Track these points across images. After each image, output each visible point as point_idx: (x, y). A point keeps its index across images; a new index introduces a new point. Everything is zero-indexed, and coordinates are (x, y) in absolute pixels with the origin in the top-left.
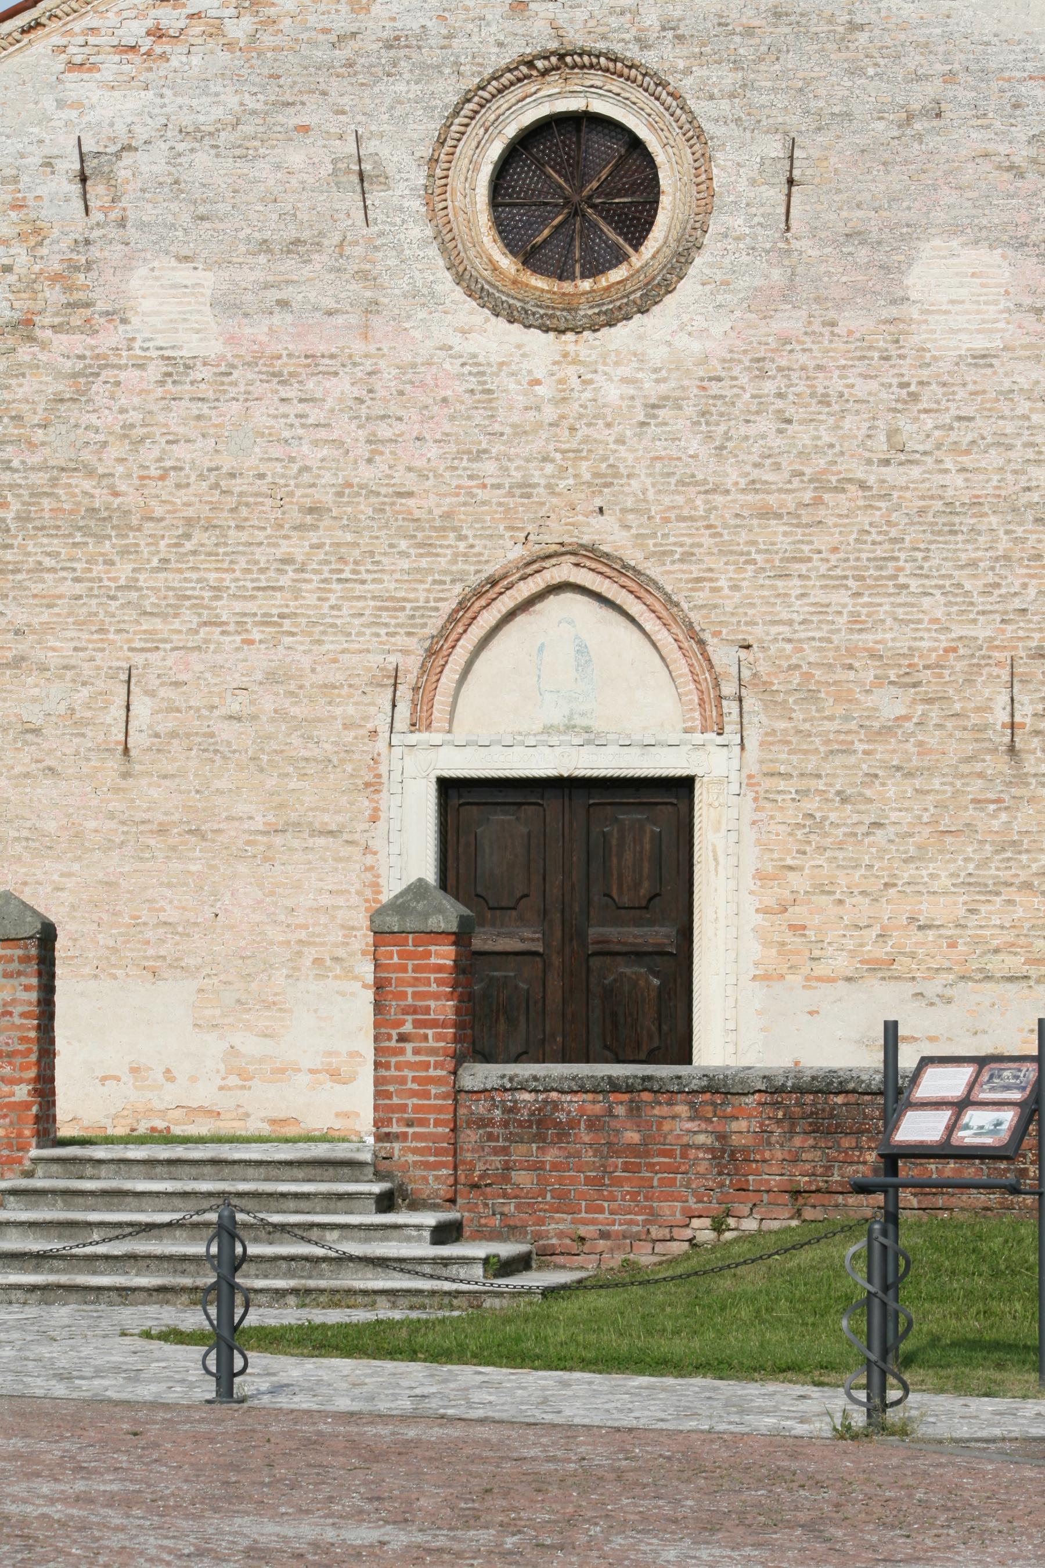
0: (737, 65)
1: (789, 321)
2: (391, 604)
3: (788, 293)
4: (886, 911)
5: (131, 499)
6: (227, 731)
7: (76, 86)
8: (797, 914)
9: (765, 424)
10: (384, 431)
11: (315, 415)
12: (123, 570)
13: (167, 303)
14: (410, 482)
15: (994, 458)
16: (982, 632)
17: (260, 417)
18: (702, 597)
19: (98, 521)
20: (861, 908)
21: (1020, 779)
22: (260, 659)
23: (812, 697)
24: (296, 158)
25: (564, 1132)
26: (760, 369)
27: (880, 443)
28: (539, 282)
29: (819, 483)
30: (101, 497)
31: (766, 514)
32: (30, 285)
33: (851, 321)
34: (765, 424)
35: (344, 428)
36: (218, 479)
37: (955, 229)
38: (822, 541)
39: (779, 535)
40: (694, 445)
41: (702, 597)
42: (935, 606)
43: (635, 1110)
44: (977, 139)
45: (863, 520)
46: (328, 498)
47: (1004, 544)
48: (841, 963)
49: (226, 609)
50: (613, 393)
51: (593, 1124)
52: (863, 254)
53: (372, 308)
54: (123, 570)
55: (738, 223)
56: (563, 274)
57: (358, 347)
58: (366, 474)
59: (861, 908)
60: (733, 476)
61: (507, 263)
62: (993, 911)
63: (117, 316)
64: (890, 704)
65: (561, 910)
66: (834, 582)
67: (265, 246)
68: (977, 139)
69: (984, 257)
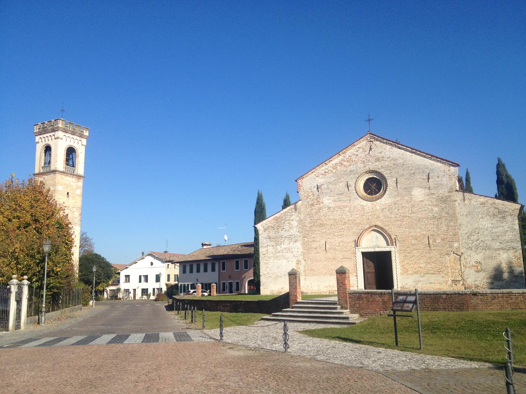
0: (390, 170)
1: (398, 198)
2: (354, 232)
3: (398, 195)
4: (415, 266)
5: (325, 222)
6: (337, 247)
7: (317, 179)
8: (405, 266)
9: (396, 210)
10: (352, 213)
11: (344, 212)
12: (325, 230)
13: (327, 201)
14: (356, 219)
15: (425, 212)
16: (424, 233)
17: (338, 213)
18: (390, 230)
19: (321, 225)
20: (412, 266)
21: (430, 250)
22: (340, 240)
23: (404, 241)
24: (341, 184)
25: (362, 299)
26: (395, 204)
27: (410, 212)
28: (369, 196)
29: (403, 217)
30: (322, 222)
31: (397, 220)
32: (313, 200)
33: (406, 198)
34: (396, 210)
35: (348, 214)
36: (335, 220)
37: (417, 187)
38: (404, 223)
39: (399, 223)
40: (388, 213)
41: (390, 230)
42: (418, 230)
43: (371, 296)
44: (419, 177)
45: (409, 220)
46: (346, 221)
47: (426, 222)
48: (411, 272)
49: (336, 234)
50: (378, 208)
51: (366, 297)
52: (406, 190)
53: (350, 200)
54: (325, 230)
55: (391, 188)
56: (372, 195)
57: (349, 204)
58: (351, 218)
59: (412, 266)
60: (393, 216)
61: (365, 194)
62: (429, 266)
63: (323, 203)
64: (414, 242)
65: (379, 266)
66: (406, 228)
67: (338, 194)
68: (419, 177)
69: (420, 189)
